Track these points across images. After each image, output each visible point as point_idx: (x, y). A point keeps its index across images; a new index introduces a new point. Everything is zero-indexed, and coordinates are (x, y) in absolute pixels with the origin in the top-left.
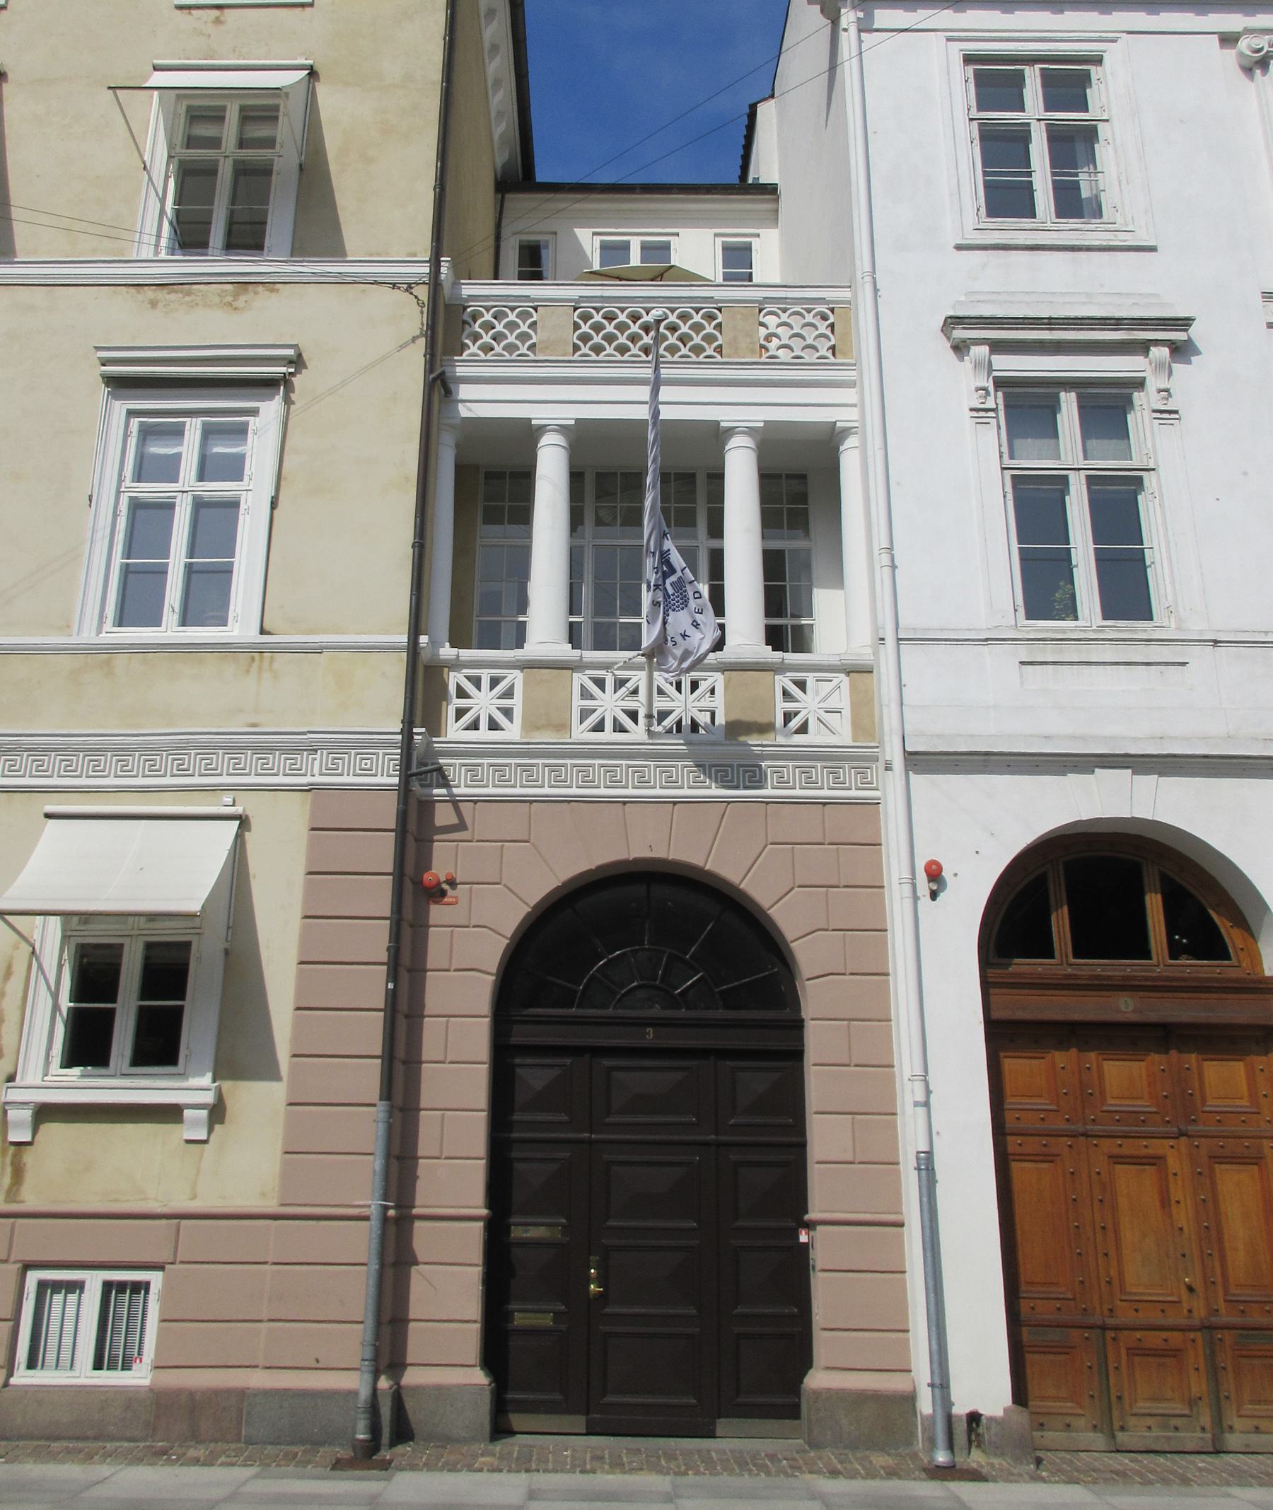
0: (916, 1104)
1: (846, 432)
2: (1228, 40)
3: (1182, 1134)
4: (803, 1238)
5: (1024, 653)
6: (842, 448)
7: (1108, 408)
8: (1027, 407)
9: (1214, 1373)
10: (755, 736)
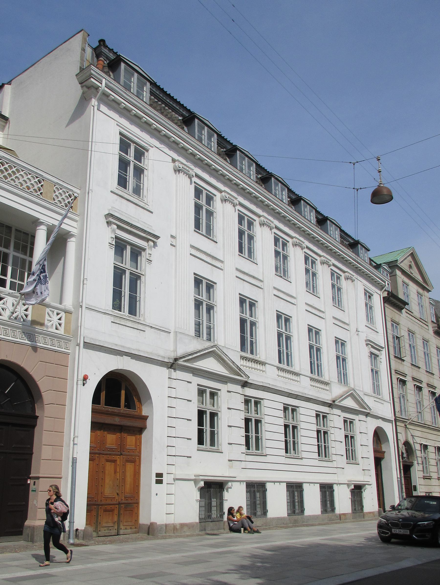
0: (77, 444)
1: (73, 236)
2: (174, 161)
3: (121, 454)
4: (29, 482)
5: (113, 319)
6: (69, 240)
7: (137, 253)
8: (120, 246)
9: (119, 515)
10: (39, 326)
